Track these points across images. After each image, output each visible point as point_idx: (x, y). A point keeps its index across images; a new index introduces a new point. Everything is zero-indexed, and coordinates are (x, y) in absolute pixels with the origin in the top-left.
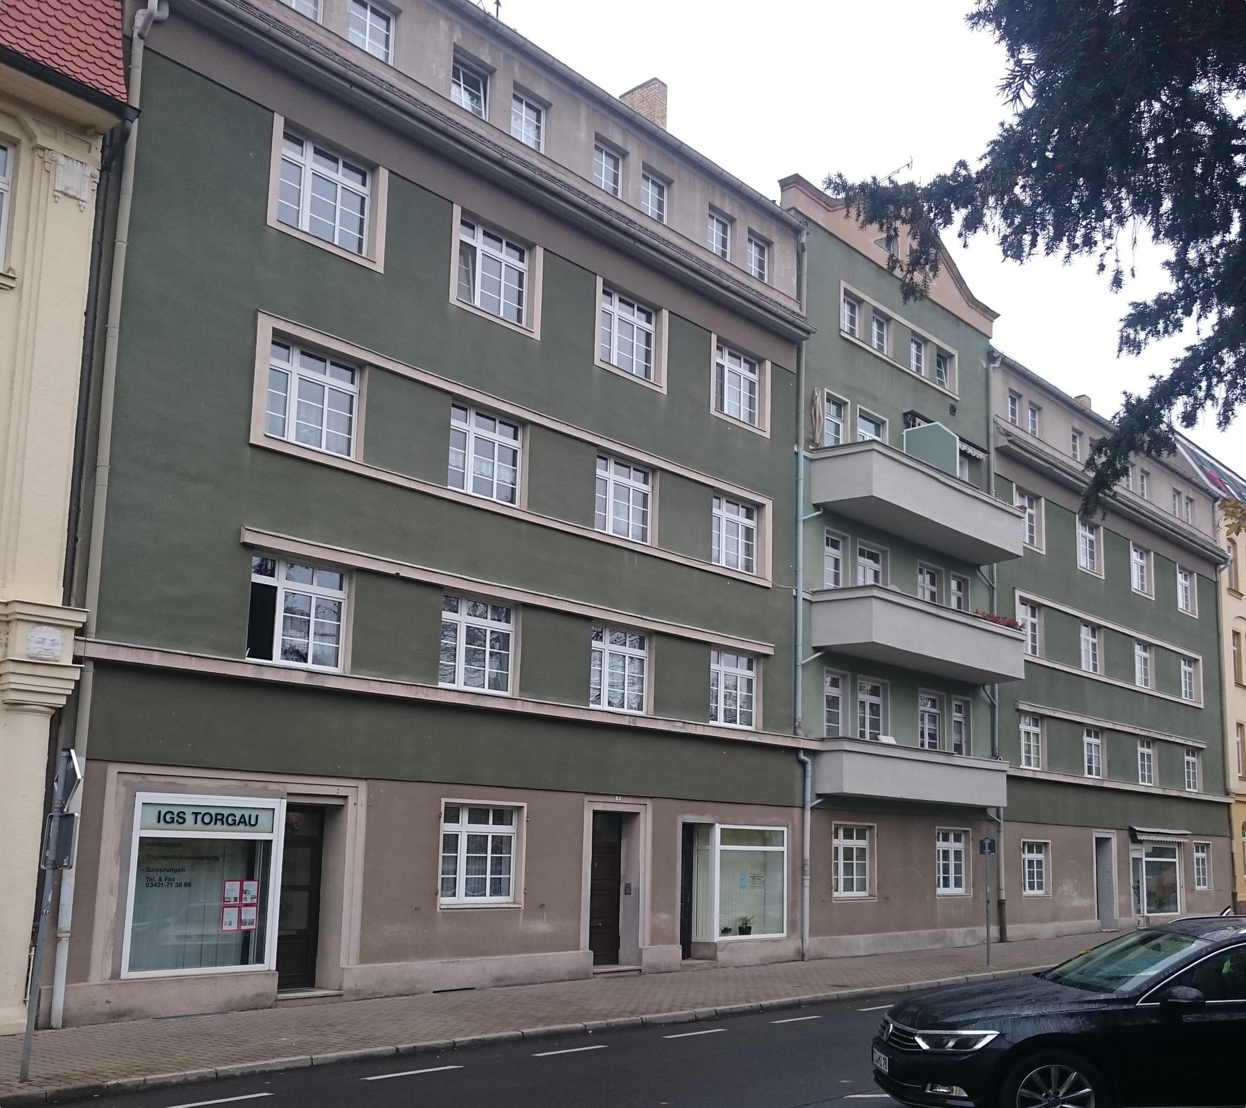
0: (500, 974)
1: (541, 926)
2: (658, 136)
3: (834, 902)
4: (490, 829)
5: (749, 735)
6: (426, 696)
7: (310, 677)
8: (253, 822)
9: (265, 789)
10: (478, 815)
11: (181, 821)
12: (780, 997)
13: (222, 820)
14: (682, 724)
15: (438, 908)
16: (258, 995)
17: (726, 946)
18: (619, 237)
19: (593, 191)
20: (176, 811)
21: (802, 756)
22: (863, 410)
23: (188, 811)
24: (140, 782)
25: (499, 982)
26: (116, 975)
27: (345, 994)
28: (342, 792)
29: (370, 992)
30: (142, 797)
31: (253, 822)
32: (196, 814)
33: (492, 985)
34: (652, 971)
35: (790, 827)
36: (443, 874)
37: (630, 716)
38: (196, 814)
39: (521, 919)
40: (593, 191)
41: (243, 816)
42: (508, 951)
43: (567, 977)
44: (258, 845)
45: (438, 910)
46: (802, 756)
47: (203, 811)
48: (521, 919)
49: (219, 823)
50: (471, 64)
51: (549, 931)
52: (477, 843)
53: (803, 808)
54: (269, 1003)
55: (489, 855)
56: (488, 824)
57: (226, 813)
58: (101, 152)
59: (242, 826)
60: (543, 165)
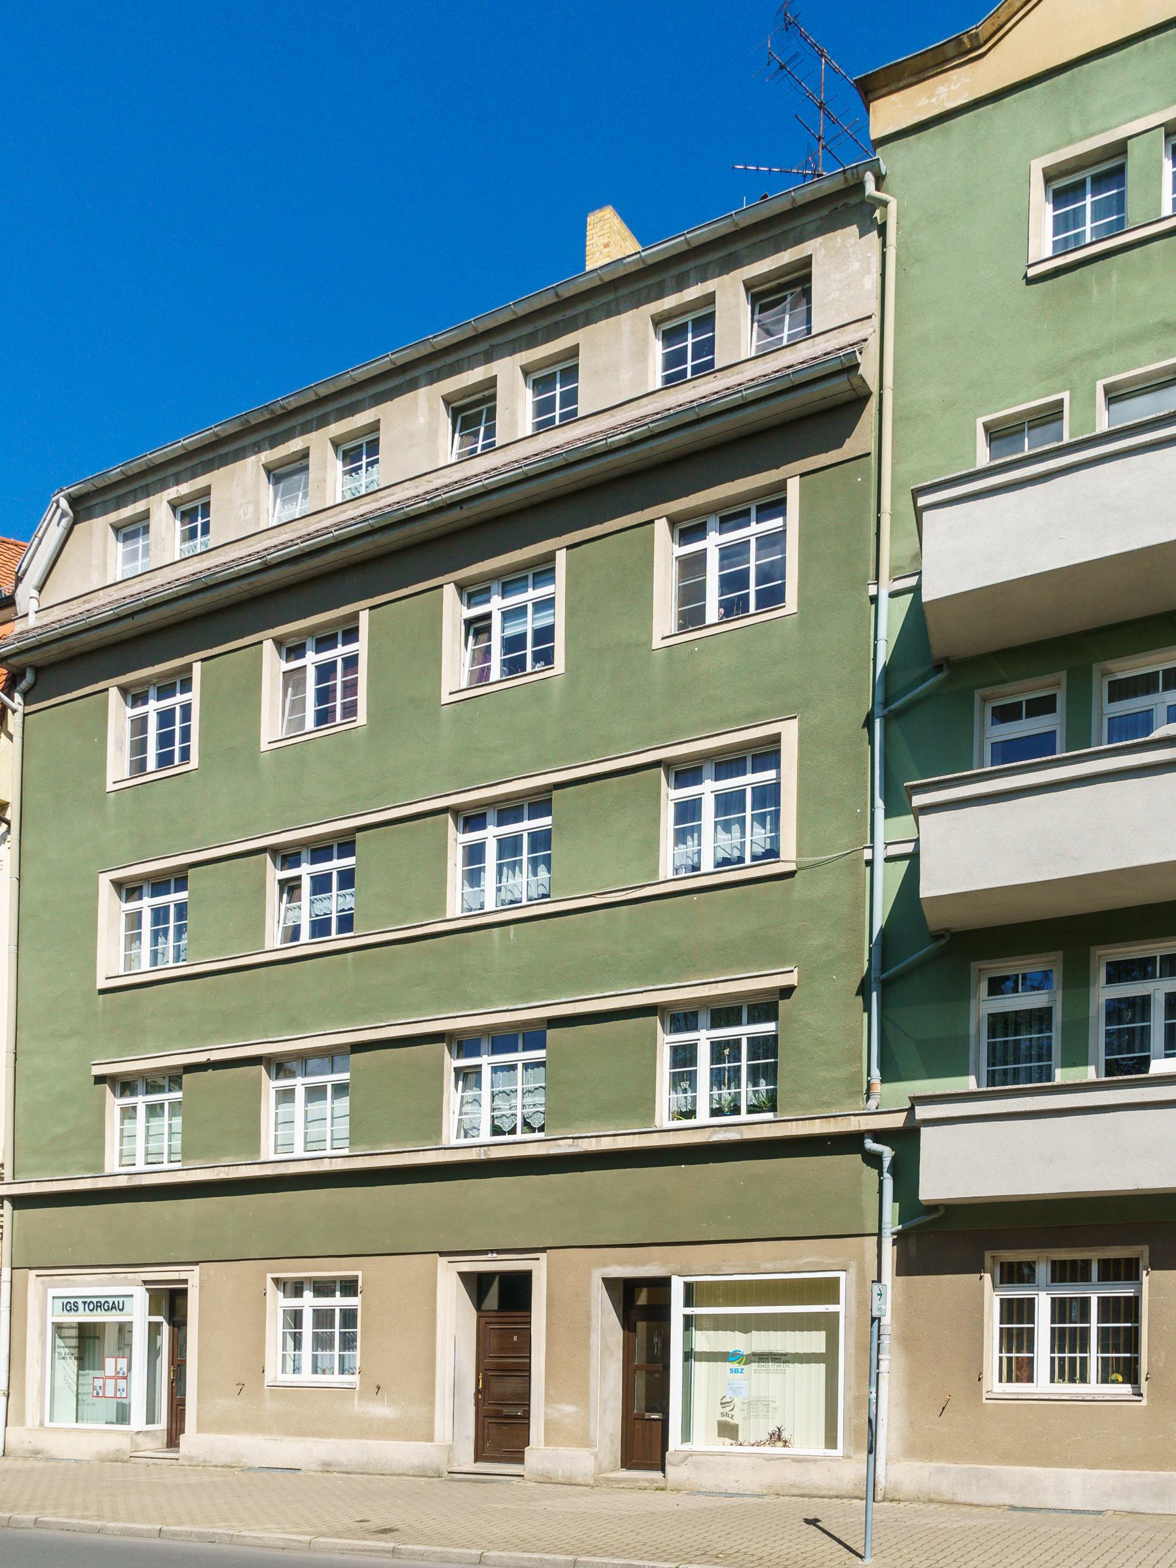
0: (328, 1459)
1: (381, 1410)
3: (984, 1401)
5: (716, 1132)
6: (228, 1174)
7: (130, 1179)
8: (121, 1308)
9: (126, 1278)
10: (323, 1288)
11: (75, 1309)
13: (100, 1306)
16: (118, 1450)
17: (686, 1458)
19: (429, 481)
20: (72, 1301)
21: (869, 1144)
22: (484, 436)
23: (80, 1301)
24: (49, 1281)
25: (327, 1467)
26: (42, 1424)
27: (180, 1458)
28: (183, 1276)
29: (202, 1460)
31: (121, 1308)
32: (85, 1303)
33: (319, 1469)
34: (542, 1479)
35: (853, 1271)
36: (688, 1303)
38: (85, 1303)
39: (356, 1402)
40: (429, 481)
41: (114, 1302)
42: (341, 1435)
43: (411, 1472)
45: (266, 1387)
46: (869, 1144)
47: (88, 1300)
48: (356, 1402)
49: (99, 1309)
50: (483, 394)
53: (879, 1235)
54: (126, 1458)
56: (150, 1314)
57: (103, 1300)
58: (869, 743)
59: (114, 1311)
60: (361, 508)
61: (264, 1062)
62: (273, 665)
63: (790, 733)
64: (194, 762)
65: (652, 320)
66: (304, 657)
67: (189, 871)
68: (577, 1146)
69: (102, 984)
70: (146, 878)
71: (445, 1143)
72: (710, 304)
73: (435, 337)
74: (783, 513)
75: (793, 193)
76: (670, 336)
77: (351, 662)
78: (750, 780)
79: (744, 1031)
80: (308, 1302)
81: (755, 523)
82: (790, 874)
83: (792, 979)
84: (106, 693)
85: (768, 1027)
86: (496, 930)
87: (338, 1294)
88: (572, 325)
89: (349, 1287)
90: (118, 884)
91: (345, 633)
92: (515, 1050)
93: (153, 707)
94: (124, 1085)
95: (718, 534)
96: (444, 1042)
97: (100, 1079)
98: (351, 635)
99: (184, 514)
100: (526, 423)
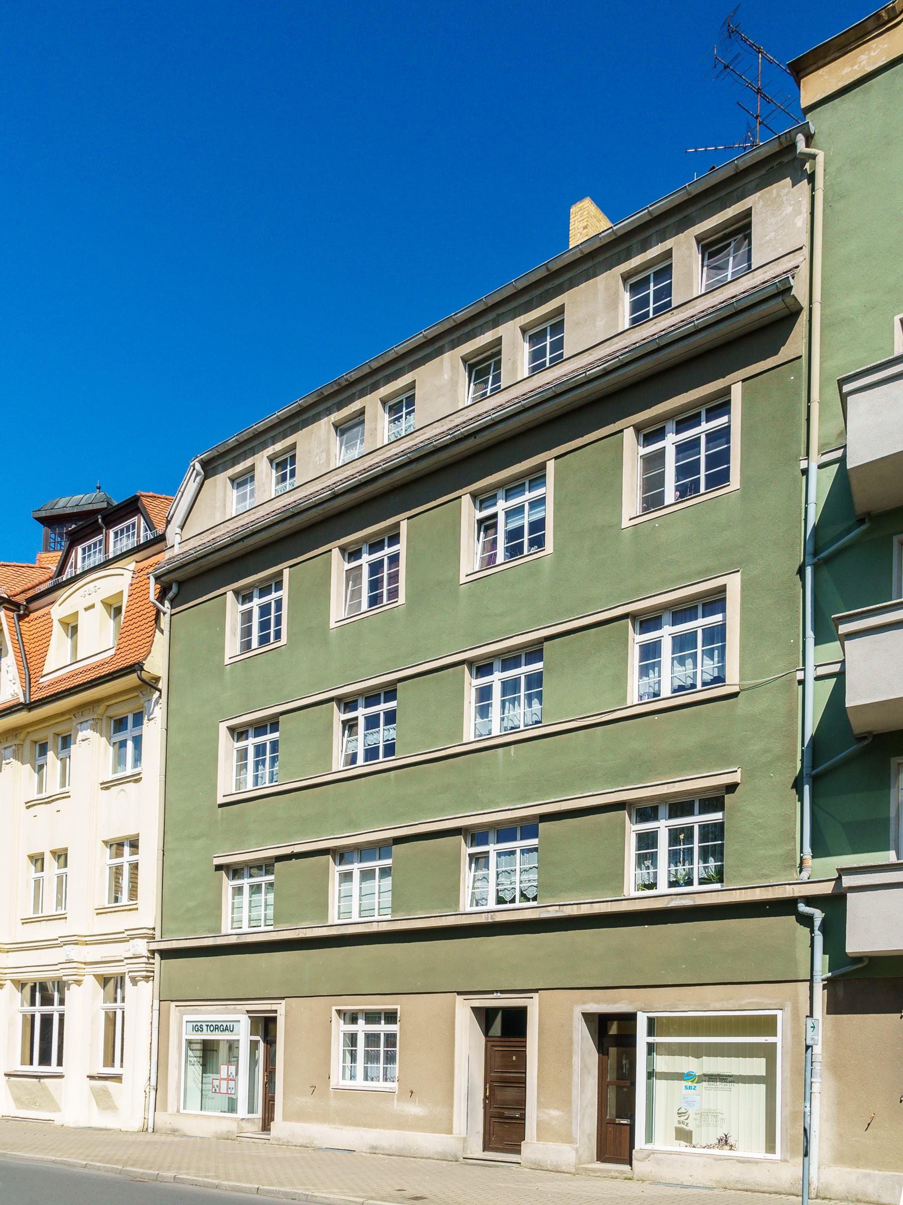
1: (413, 1109)
2: (284, 417)
4: (383, 1028)
8: (231, 1029)
9: (235, 1008)
12: (272, 1185)
14: (558, 907)
15: (331, 1088)
16: (228, 1132)
18: (579, 393)
20: (199, 1024)
21: (802, 908)
23: (204, 1024)
25: (374, 1150)
26: (178, 1111)
28: (274, 1007)
29: (286, 1140)
30: (186, 1018)
31: (231, 1029)
32: (207, 1026)
37: (488, 912)
38: (207, 1026)
39: (395, 1102)
40: (451, 421)
42: (384, 1127)
44: (221, 1043)
46: (802, 908)
47: (210, 1024)
48: (395, 1102)
49: (217, 1030)
50: (491, 351)
51: (422, 1114)
52: (372, 1039)
53: (811, 981)
55: (382, 1049)
60: (402, 446)
61: (224, 869)
62: (233, 609)
63: (734, 584)
64: (284, 640)
65: (622, 277)
66: (361, 558)
67: (280, 717)
68: (562, 911)
69: (221, 800)
70: (250, 724)
71: (461, 911)
72: (293, 450)
73: (456, 314)
74: (728, 412)
75: (736, 162)
76: (634, 288)
77: (279, 602)
78: (700, 623)
79: (696, 820)
80: (362, 1028)
81: (705, 422)
82: (735, 695)
83: (736, 778)
84: (224, 596)
85: (717, 816)
86: (500, 750)
87: (383, 1022)
88: (560, 290)
89: (391, 1017)
90: (232, 730)
91: (390, 538)
92: (515, 840)
93: (256, 603)
94: (235, 871)
95: (674, 434)
96: (461, 835)
97: (219, 868)
98: (394, 539)
99: (278, 465)
100: (524, 370)
